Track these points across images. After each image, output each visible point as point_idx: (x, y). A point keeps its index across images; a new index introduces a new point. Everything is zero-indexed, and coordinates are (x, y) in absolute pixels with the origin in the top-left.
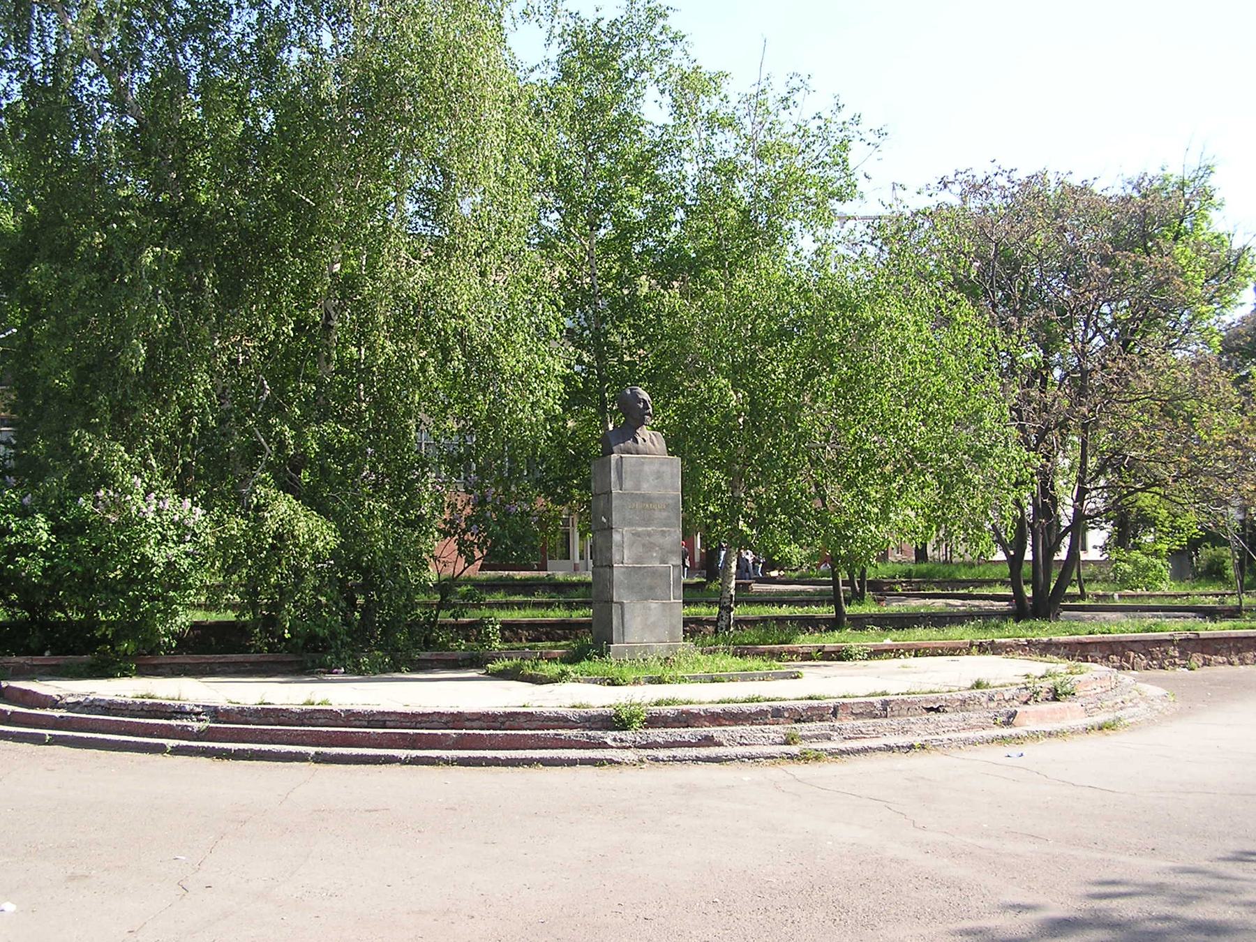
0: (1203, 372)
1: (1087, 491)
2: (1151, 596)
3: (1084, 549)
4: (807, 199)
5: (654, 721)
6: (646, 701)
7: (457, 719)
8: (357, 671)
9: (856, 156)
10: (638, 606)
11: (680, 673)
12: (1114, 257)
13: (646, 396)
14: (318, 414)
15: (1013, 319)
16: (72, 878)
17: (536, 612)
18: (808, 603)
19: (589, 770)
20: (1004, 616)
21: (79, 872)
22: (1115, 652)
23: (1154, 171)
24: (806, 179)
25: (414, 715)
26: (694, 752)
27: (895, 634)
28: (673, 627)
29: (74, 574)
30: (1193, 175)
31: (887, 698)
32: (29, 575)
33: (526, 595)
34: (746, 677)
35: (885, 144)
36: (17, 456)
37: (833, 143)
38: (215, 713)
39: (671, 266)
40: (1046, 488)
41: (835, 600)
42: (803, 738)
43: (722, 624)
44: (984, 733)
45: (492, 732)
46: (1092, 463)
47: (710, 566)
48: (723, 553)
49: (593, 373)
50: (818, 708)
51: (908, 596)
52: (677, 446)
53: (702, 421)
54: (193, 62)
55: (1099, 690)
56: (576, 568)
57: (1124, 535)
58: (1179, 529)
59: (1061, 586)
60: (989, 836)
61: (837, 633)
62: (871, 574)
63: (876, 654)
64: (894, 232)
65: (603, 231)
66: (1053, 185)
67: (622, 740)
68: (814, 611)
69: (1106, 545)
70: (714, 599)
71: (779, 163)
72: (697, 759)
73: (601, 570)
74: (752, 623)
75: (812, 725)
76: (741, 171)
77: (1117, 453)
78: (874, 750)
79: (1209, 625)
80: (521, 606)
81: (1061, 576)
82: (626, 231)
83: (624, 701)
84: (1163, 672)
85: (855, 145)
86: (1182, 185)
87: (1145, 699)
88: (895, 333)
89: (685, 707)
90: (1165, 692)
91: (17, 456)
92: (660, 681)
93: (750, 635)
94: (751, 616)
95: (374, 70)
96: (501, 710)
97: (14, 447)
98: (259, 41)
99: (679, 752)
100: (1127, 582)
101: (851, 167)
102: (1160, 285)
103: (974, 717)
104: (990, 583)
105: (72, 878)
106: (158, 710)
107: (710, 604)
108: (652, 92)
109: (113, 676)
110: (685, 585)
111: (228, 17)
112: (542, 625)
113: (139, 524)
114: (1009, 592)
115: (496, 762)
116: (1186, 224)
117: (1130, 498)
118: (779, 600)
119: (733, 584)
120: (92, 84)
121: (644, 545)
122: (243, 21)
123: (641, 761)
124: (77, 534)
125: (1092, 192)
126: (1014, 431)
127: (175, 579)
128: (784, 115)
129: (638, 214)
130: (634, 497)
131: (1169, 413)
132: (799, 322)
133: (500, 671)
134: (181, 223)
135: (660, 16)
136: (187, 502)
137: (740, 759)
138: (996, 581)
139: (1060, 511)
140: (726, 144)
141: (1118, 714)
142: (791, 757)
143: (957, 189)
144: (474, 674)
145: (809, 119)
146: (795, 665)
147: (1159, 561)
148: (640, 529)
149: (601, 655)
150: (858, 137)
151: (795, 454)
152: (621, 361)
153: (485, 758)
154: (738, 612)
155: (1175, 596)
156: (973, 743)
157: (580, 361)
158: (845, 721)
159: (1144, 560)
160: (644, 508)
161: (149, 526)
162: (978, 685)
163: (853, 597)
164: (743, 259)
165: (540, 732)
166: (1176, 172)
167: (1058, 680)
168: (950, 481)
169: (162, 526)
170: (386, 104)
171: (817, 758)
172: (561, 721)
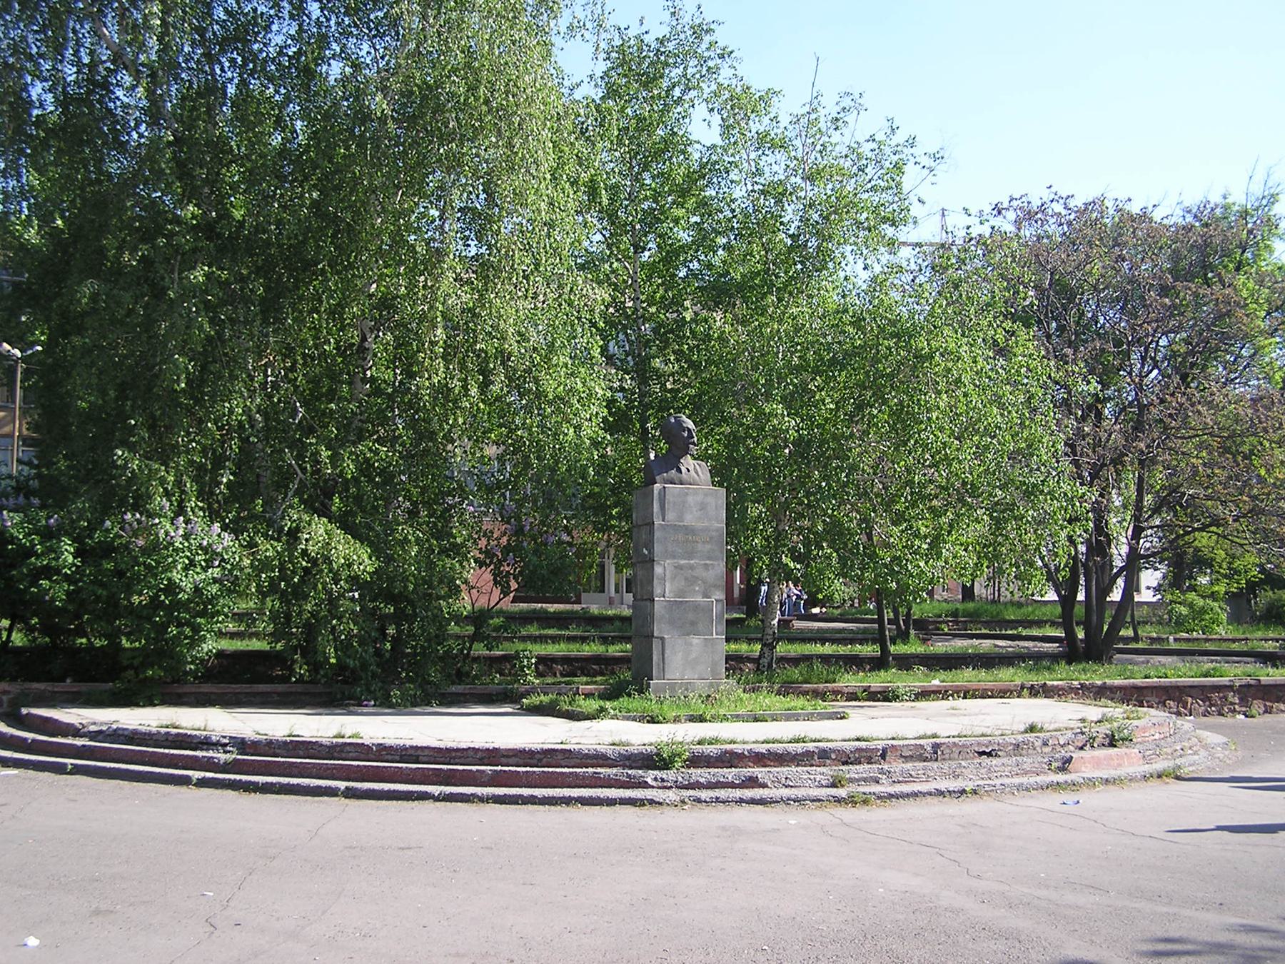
0: (1265, 407)
1: (1143, 529)
2: (1207, 640)
3: (1138, 590)
4: (859, 224)
5: (697, 761)
6: (688, 740)
7: (492, 756)
8: (386, 703)
9: (910, 179)
10: (679, 641)
11: (722, 712)
12: (1174, 287)
13: (690, 424)
14: (346, 439)
15: (1069, 351)
16: (97, 912)
17: (571, 646)
18: (852, 641)
19: (629, 810)
20: (1055, 658)
21: (103, 907)
22: (1171, 697)
23: (1216, 198)
24: (857, 201)
25: (449, 750)
26: (738, 793)
27: (943, 675)
28: (714, 665)
29: (98, 598)
30: (1256, 204)
31: (938, 740)
32: (53, 600)
33: (560, 629)
34: (791, 716)
35: (940, 169)
36: (39, 476)
37: (887, 165)
38: (242, 745)
39: (719, 293)
40: (1101, 528)
41: (880, 639)
42: (851, 780)
43: (765, 661)
44: (1038, 779)
45: (528, 769)
46: (1148, 499)
48: (764, 588)
50: (867, 750)
51: (955, 636)
53: (749, 450)
54: (229, 74)
55: (1157, 736)
57: (1180, 576)
58: (1237, 572)
59: (1115, 627)
60: (1047, 887)
61: (882, 673)
62: (916, 612)
63: (924, 695)
64: (942, 259)
65: (647, 254)
66: (1111, 211)
67: (663, 780)
68: (860, 650)
69: (1160, 585)
70: (753, 636)
71: (830, 186)
72: (741, 801)
74: (795, 661)
76: (791, 194)
77: (1175, 491)
78: (924, 794)
79: (1271, 670)
80: (555, 639)
81: (1115, 618)
82: (671, 255)
83: (665, 739)
84: (1221, 720)
85: (910, 169)
86: (1245, 214)
87: (1205, 747)
88: (950, 365)
90: (1225, 740)
91: (39, 476)
92: (701, 719)
93: (795, 673)
94: (793, 654)
95: (416, 85)
96: (539, 747)
97: (37, 467)
98: (299, 53)
99: (722, 793)
100: (1182, 624)
101: (905, 191)
102: (1221, 317)
103: (1028, 762)
104: (1039, 623)
105: (97, 912)
106: (183, 741)
107: (750, 641)
108: (700, 111)
109: (137, 705)
111: (267, 29)
112: (577, 659)
113: (166, 548)
114: (1060, 633)
115: (532, 800)
116: (1248, 255)
117: (1186, 538)
118: (821, 637)
120: (127, 95)
121: (686, 579)
122: (280, 35)
123: (683, 802)
124: (101, 558)
125: (1151, 220)
126: (1066, 464)
127: (202, 605)
128: (836, 137)
129: (684, 236)
131: (1227, 450)
132: (855, 352)
133: (535, 707)
134: (217, 238)
135: (707, 31)
136: (216, 527)
137: (786, 801)
138: (1046, 622)
139: (1114, 551)
140: (775, 166)
141: (1178, 762)
142: (839, 800)
143: (1011, 215)
144: (510, 710)
145: (861, 140)
147: (1216, 604)
148: (682, 562)
149: (641, 692)
150: (912, 160)
151: (845, 485)
154: (782, 649)
155: (1234, 641)
156: (1027, 789)
158: (894, 764)
159: (1201, 602)
160: (687, 541)
161: (176, 550)
162: (1032, 729)
163: (898, 636)
164: (790, 289)
166: (1238, 199)
167: (1115, 724)
168: (1001, 515)
169: (190, 550)
170: (433, 122)
171: (865, 802)
172: (599, 759)
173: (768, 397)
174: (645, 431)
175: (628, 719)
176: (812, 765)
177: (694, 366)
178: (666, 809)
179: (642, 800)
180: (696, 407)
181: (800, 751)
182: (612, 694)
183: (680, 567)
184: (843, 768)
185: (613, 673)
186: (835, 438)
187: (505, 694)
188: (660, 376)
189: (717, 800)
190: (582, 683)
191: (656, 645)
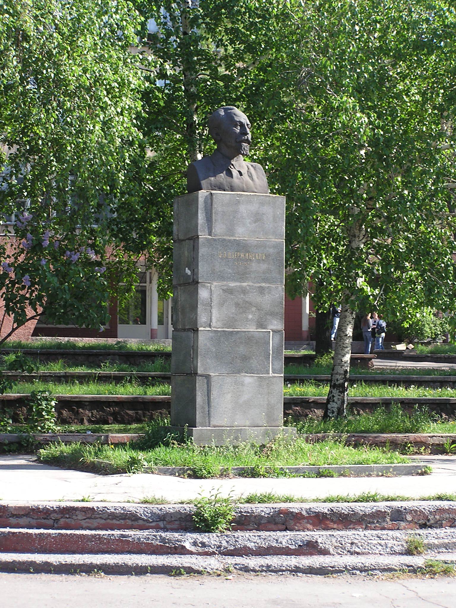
5: (244, 522)
11: (278, 465)
13: (243, 118)
26: (293, 561)
28: (270, 408)
33: (89, 367)
34: (362, 470)
42: (430, 547)
43: (334, 406)
45: (42, 531)
47: (320, 334)
48: (337, 320)
49: (179, 89)
52: (283, 181)
53: (316, 150)
56: (153, 335)
67: (203, 545)
72: (296, 570)
73: (184, 334)
75: (440, 532)
80: (83, 379)
89: (283, 506)
92: (253, 473)
93: (366, 420)
96: (55, 505)
99: (274, 561)
107: (319, 382)
110: (288, 360)
112: (108, 403)
118: (405, 380)
119: (347, 358)
121: (237, 305)
123: (227, 571)
130: (225, 244)
137: (351, 570)
142: (414, 570)
144: (23, 462)
146: (422, 459)
148: (232, 284)
151: (433, 195)
152: (215, 75)
153: (47, 564)
154: (354, 392)
157: (162, 75)
160: (238, 259)
165: (102, 532)
173: (338, 87)
174: (191, 125)
175: (165, 472)
176: (383, 529)
177: (251, 48)
178: (206, 579)
179: (178, 568)
180: (253, 98)
181: (368, 511)
182: (146, 444)
183: (229, 291)
184: (421, 531)
185: (151, 418)
186: (421, 136)
187: (19, 443)
188: (209, 60)
189: (269, 569)
190: (116, 433)
191: (200, 384)
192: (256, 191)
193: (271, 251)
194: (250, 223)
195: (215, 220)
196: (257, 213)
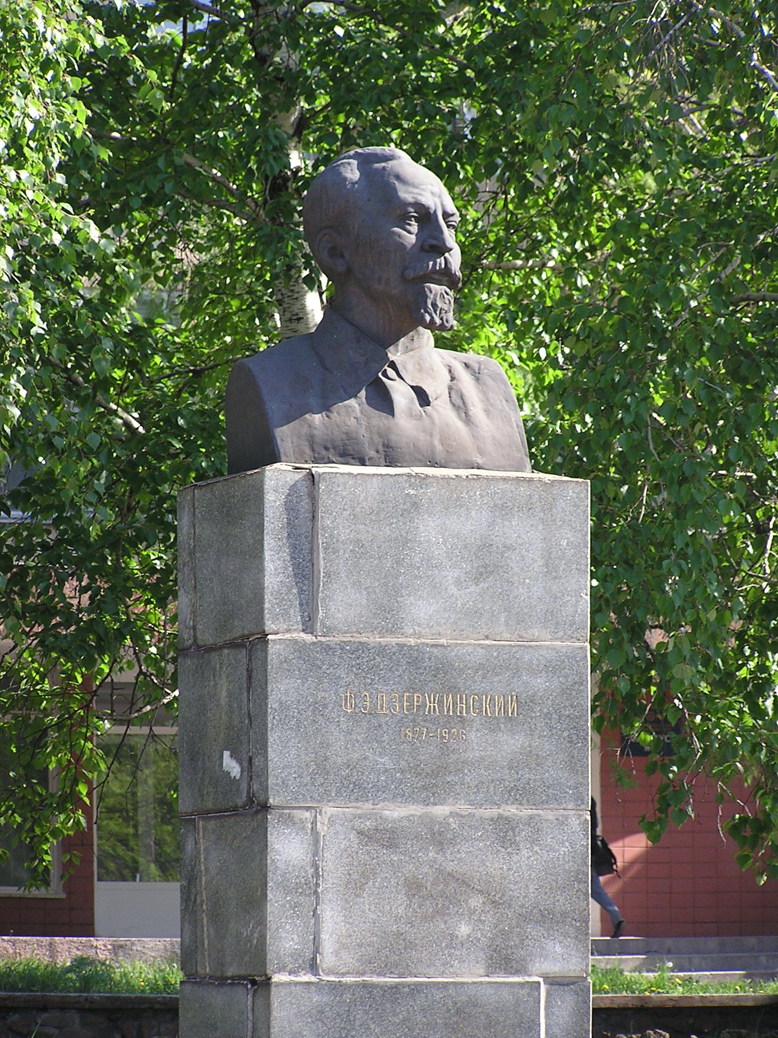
121: (414, 887)
148: (395, 812)
183: (384, 837)
192: (480, 461)
193: (540, 683)
194: (458, 582)
195: (328, 575)
196: (486, 546)
